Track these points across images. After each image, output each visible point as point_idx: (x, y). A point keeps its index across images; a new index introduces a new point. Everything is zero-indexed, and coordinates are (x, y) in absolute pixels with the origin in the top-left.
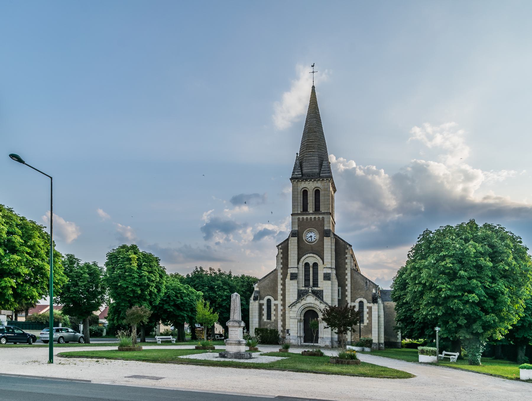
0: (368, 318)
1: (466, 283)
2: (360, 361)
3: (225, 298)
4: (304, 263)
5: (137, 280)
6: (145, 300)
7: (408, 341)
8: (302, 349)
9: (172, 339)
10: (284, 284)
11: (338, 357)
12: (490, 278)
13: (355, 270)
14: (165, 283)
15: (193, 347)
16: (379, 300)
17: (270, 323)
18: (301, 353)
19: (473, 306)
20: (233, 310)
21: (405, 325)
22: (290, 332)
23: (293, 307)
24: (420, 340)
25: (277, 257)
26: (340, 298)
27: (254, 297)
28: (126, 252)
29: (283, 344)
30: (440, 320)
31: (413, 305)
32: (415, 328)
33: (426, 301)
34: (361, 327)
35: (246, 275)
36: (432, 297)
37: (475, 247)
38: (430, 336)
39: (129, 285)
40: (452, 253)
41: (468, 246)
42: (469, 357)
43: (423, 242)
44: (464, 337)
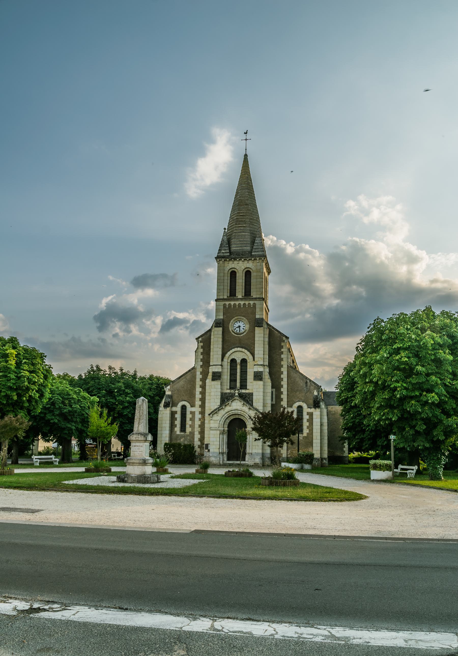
0: (308, 427)
1: (424, 380)
2: (299, 481)
3: (126, 405)
4: (230, 359)
5: (14, 382)
6: (22, 408)
7: (356, 454)
8: (224, 469)
9: (54, 459)
10: (203, 387)
11: (271, 477)
12: (450, 374)
13: (293, 368)
14: (50, 386)
15: (83, 469)
16: (322, 405)
17: (184, 437)
18: (224, 474)
19: (433, 407)
20: (138, 420)
21: (353, 435)
22: (210, 447)
24: (370, 452)
25: (196, 352)
26: (274, 403)
27: (165, 403)
28: (2, 347)
29: (200, 462)
30: (395, 426)
31: (362, 409)
32: (365, 438)
33: (378, 404)
34: (300, 438)
35: (155, 375)
36: (385, 398)
37: (432, 338)
38: (383, 447)
39: (3, 388)
40: (408, 345)
41: (425, 336)
42: (430, 471)
43: (373, 332)
44: (424, 446)
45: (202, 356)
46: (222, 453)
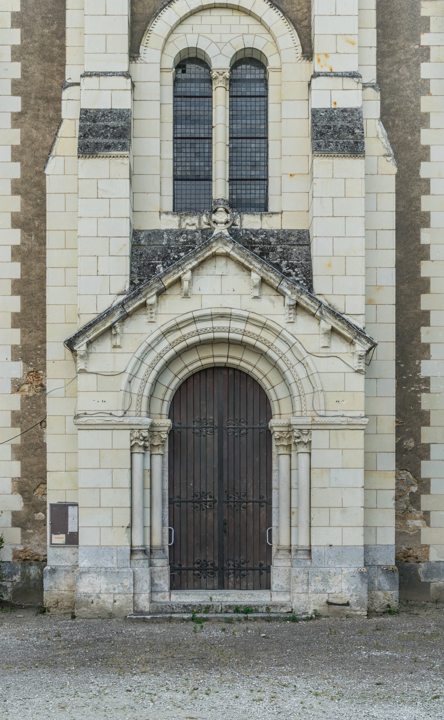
23: (98, 348)
45: (18, 66)
46: (144, 552)
